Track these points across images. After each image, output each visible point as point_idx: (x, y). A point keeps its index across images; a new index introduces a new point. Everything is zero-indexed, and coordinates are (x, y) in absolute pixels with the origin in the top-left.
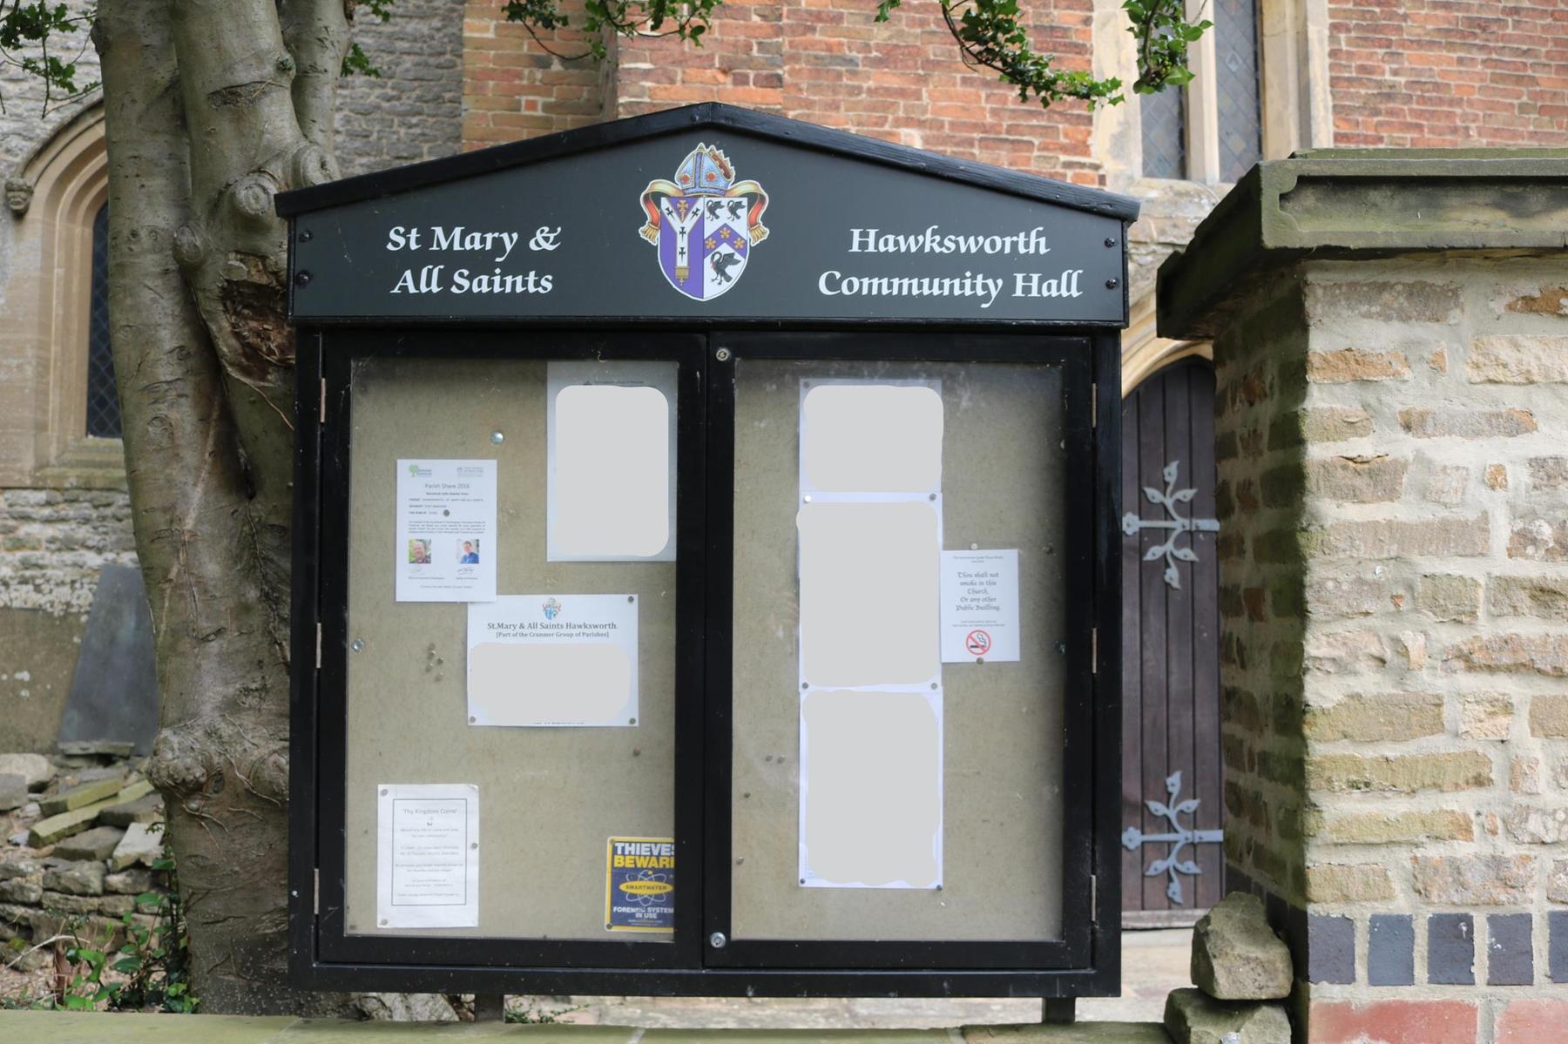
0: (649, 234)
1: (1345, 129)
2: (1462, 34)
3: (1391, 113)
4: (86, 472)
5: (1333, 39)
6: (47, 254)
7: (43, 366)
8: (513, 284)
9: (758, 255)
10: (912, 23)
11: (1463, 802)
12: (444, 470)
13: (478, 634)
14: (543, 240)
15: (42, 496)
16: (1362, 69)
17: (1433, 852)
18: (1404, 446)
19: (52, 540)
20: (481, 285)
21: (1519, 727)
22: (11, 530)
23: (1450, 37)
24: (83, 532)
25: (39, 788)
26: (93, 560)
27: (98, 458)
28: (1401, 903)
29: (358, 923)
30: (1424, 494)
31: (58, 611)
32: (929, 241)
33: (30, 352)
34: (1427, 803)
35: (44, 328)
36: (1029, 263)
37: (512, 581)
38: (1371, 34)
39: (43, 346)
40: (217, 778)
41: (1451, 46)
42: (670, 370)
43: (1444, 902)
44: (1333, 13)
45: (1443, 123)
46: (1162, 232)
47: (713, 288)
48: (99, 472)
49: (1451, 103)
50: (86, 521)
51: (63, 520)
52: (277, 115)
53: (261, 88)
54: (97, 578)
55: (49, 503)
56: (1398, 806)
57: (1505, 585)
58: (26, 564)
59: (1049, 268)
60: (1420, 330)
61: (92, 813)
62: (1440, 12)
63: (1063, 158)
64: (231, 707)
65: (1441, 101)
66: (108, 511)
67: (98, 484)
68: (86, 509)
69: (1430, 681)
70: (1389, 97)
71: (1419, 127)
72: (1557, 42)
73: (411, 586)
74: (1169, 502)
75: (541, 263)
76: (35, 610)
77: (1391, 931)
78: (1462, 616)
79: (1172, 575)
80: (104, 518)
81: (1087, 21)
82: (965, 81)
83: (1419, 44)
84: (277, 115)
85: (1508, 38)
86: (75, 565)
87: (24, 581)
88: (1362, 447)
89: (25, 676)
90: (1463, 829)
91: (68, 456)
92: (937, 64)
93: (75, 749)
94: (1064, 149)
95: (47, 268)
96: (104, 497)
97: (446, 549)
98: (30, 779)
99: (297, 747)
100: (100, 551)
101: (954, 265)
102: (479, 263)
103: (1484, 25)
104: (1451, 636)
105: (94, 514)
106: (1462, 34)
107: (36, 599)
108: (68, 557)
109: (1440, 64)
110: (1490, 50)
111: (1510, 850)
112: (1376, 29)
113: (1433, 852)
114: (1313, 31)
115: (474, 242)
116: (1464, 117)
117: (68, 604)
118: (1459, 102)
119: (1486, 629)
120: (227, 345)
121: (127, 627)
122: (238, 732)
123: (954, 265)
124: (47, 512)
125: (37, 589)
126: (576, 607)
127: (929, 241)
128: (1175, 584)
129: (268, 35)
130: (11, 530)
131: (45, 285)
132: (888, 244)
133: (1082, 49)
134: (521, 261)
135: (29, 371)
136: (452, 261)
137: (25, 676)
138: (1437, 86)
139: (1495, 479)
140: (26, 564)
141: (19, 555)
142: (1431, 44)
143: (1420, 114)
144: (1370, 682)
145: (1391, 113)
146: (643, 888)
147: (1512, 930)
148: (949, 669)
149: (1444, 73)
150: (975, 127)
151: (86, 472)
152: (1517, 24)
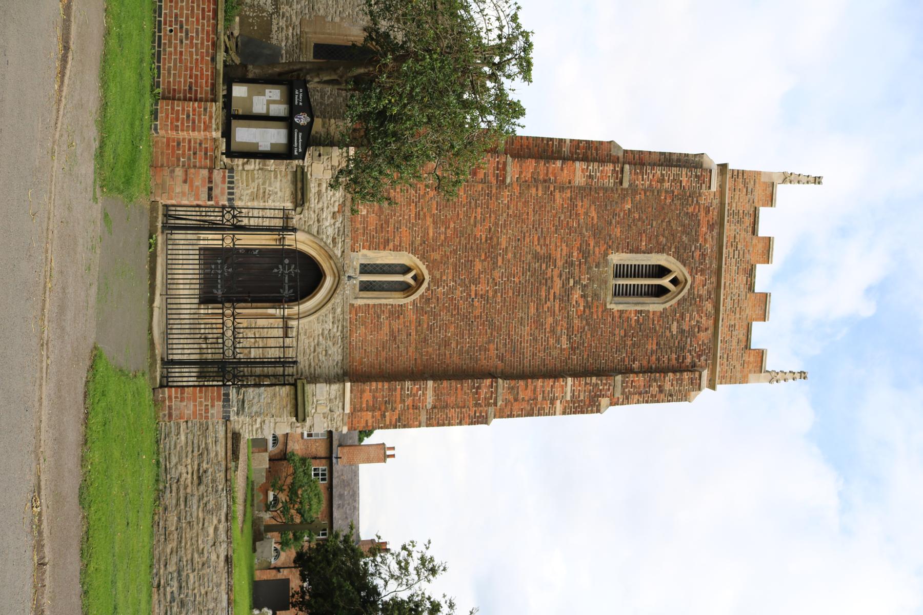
0: (301, 114)
1: (370, 307)
2: (392, 335)
3: (375, 317)
4: (304, 43)
5: (390, 305)
6: (356, 36)
7: (330, 34)
8: (296, 101)
9: (299, 124)
10: (388, 213)
11: (245, 184)
12: (279, 94)
13: (261, 98)
14: (301, 104)
15: (299, 33)
16: (384, 311)
17: (240, 181)
18: (279, 180)
19: (288, 35)
20: (296, 98)
21: (252, 190)
22: (291, 26)
23: (392, 332)
24: (290, 42)
25: (232, 34)
26: (283, 44)
27: (308, 46)
28: (235, 178)
29: (233, 84)
30: (274, 181)
31: (271, 36)
32: (300, 140)
33: (333, 31)
34: (245, 181)
35: (339, 35)
36: (298, 150)
37: (267, 100)
38: (391, 313)
39: (334, 34)
40: (247, 71)
41: (390, 332)
42: (288, 116)
43: (235, 182)
44: (395, 305)
45: (373, 329)
46: (346, 264)
47: (296, 120)
48: (304, 46)
49: (378, 331)
50: (293, 43)
51: (293, 38)
52: (316, 80)
53: (319, 77)
54: (279, 45)
55: (297, 34)
56: (244, 178)
57: (265, 189)
58: (282, 29)
59: (298, 152)
60: (290, 182)
61: (228, 46)
62: (397, 330)
63: (361, 244)
64: (255, 73)
65: (378, 329)
66: (295, 48)
67: (302, 46)
68: (296, 43)
69: (256, 181)
70: (378, 317)
71: (372, 324)
72: (392, 357)
73: (267, 91)
74: (291, 270)
75: (298, 103)
76: (271, 31)
77: (233, 177)
78: (263, 185)
79: (276, 270)
80: (293, 47)
81: (390, 250)
82: (377, 224)
83: (390, 324)
84: (316, 80)
85: (392, 346)
86: (282, 40)
87: (278, 28)
88: (279, 176)
89: (256, 28)
90: (242, 184)
91: (308, 39)
92: (380, 217)
93: (239, 39)
94: (363, 244)
95: (353, 36)
96: (298, 47)
97: (271, 94)
98: (234, 32)
99: (250, 79)
100: (285, 46)
101: (298, 142)
102: (299, 98)
103: (395, 339)
104: (261, 184)
105: (294, 45)
106: (392, 335)
107: (274, 31)
108: (284, 38)
109: (386, 329)
110: (389, 341)
111: (240, 188)
112: (392, 315)
113: (240, 181)
114: (391, 300)
115: (301, 97)
116: (375, 335)
117: (273, 38)
118: (378, 333)
119: (261, 187)
120: (293, 74)
121: (267, 52)
122: (505, 50)
123: (298, 142)
124: (295, 34)
125: (276, 31)
126: (265, 107)
127: (300, 140)
128: (274, 271)
129: (325, 79)
130: (291, 26)
131: (350, 35)
132: (300, 137)
133: (384, 249)
134: (299, 102)
135: (328, 31)
136: (299, 95)
137: (256, 28)
138: (381, 328)
139: (276, 188)
140: (282, 29)
141: (285, 27)
142: (390, 327)
143: (375, 324)
144: (256, 176)
145: (375, 317)
146: (236, 112)
147: (233, 188)
148: (258, 143)
149: (384, 330)
150: (367, 225)
151: (304, 43)
152: (395, 347)
